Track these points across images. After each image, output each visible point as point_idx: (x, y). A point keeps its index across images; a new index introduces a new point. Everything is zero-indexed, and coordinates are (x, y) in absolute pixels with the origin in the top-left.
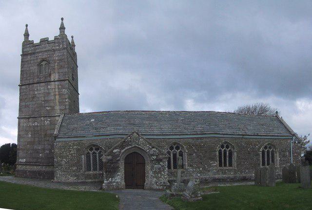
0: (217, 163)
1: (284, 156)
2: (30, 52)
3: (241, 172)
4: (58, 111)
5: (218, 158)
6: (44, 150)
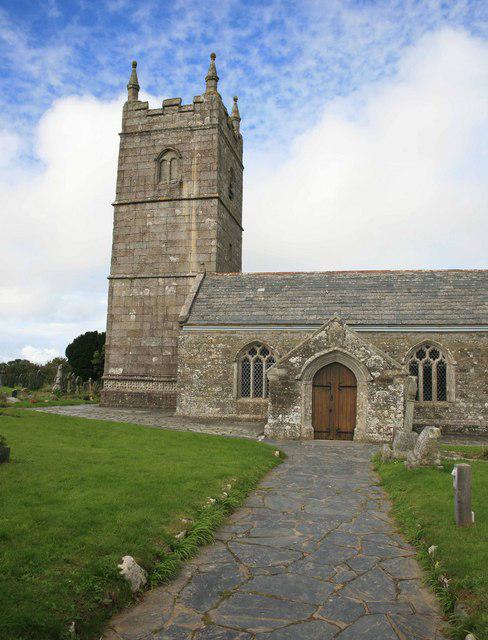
6: (161, 348)
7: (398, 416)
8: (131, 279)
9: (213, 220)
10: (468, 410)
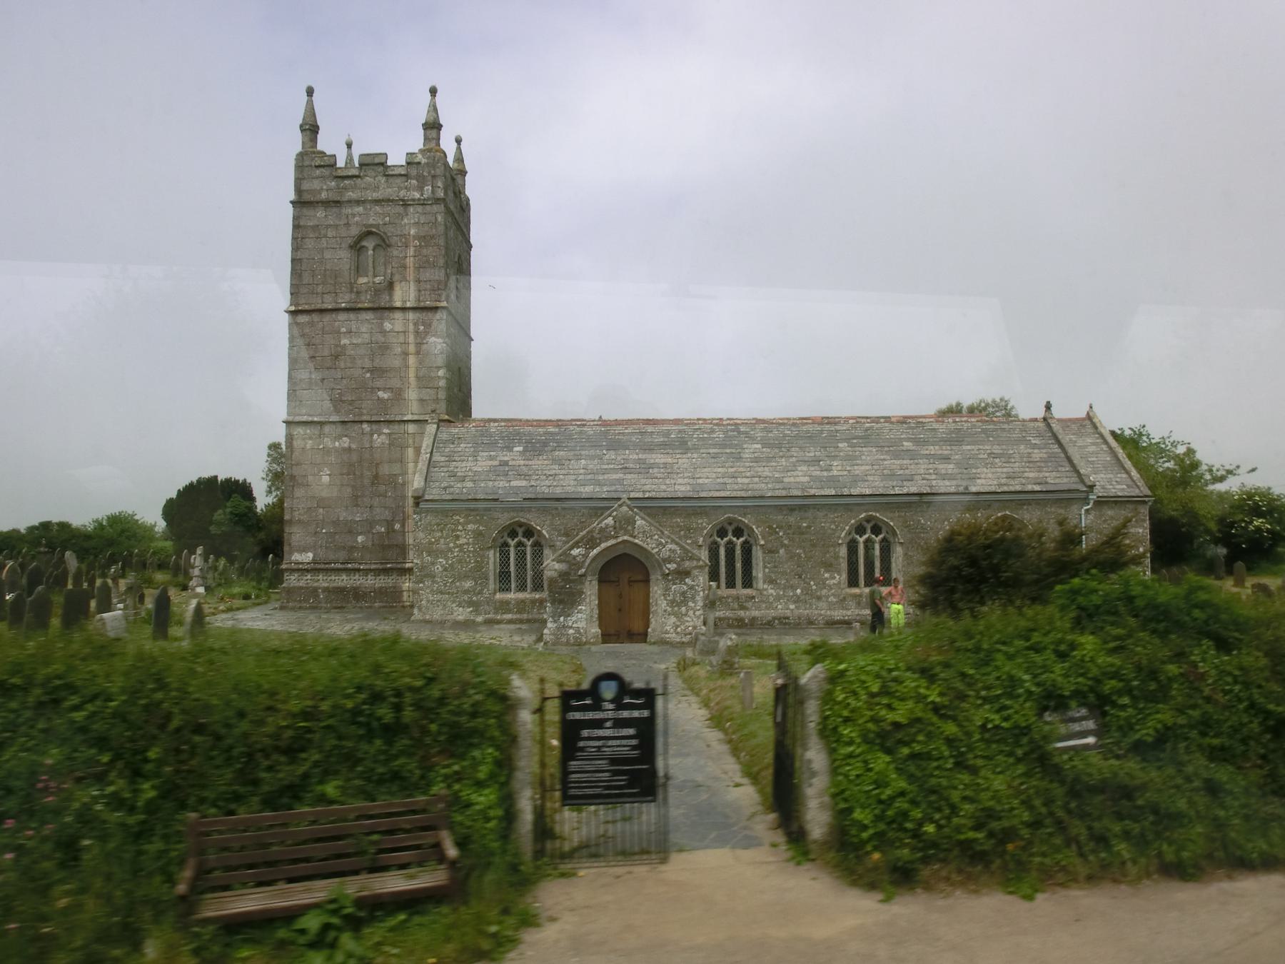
2: (324, 196)
5: (844, 565)
6: (371, 524)
7: (698, 613)
8: (321, 424)
9: (440, 340)
10: (778, 598)
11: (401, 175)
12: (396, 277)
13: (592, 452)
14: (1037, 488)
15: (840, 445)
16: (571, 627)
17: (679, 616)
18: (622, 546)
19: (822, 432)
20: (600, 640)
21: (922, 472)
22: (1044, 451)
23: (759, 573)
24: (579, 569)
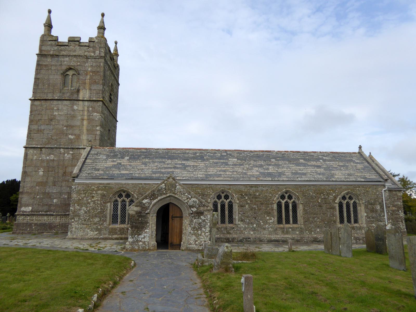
0: (274, 219)
1: (373, 211)
3: (310, 231)
4: (85, 142)
5: (276, 213)
6: (61, 193)
7: (207, 234)
8: (41, 148)
10: (245, 229)
11: (86, 46)
12: (81, 88)
13: (161, 160)
14: (363, 180)
15: (272, 160)
16: (141, 241)
17: (197, 235)
18: (169, 198)
19: (263, 155)
20: (156, 248)
21: (310, 172)
22: (362, 165)
23: (236, 216)
24: (146, 211)
